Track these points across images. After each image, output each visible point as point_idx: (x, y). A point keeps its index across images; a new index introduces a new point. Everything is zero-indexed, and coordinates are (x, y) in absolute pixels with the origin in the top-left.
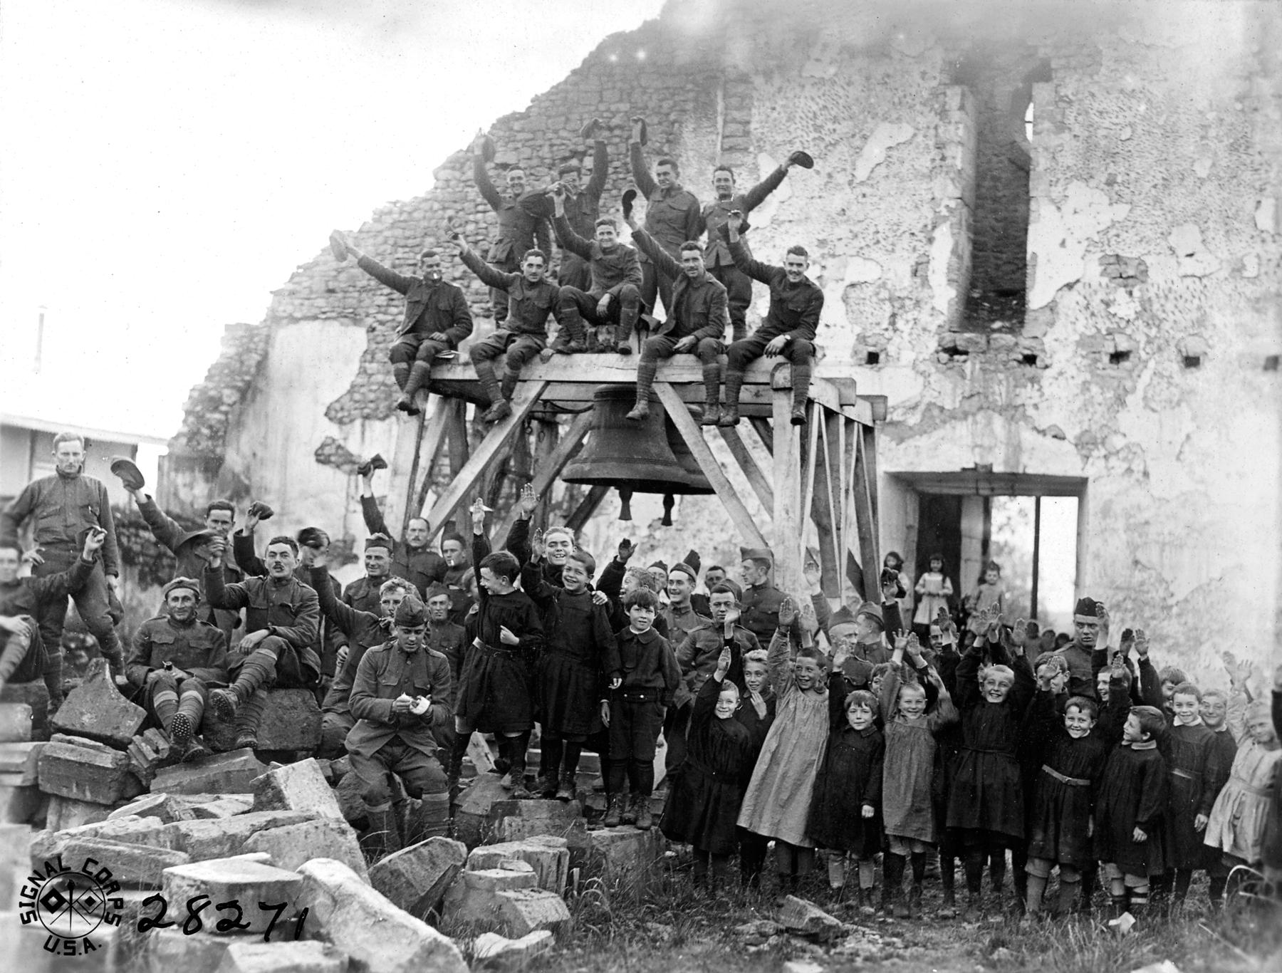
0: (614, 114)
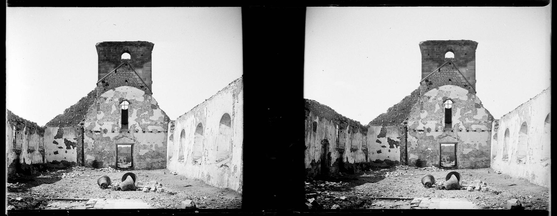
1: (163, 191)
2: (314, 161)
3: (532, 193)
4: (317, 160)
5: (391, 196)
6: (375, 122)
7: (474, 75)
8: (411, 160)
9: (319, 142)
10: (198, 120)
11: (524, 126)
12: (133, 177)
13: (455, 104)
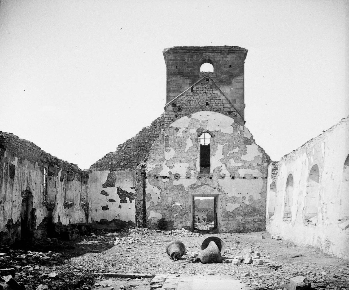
0: (146, 140)
1: (261, 263)
2: (11, 221)
3: (326, 268)
4: (15, 221)
5: (123, 272)
6: (100, 165)
7: (242, 97)
8: (150, 220)
9: (19, 194)
10: (312, 160)
11: (315, 170)
12: (219, 243)
13: (214, 138)
